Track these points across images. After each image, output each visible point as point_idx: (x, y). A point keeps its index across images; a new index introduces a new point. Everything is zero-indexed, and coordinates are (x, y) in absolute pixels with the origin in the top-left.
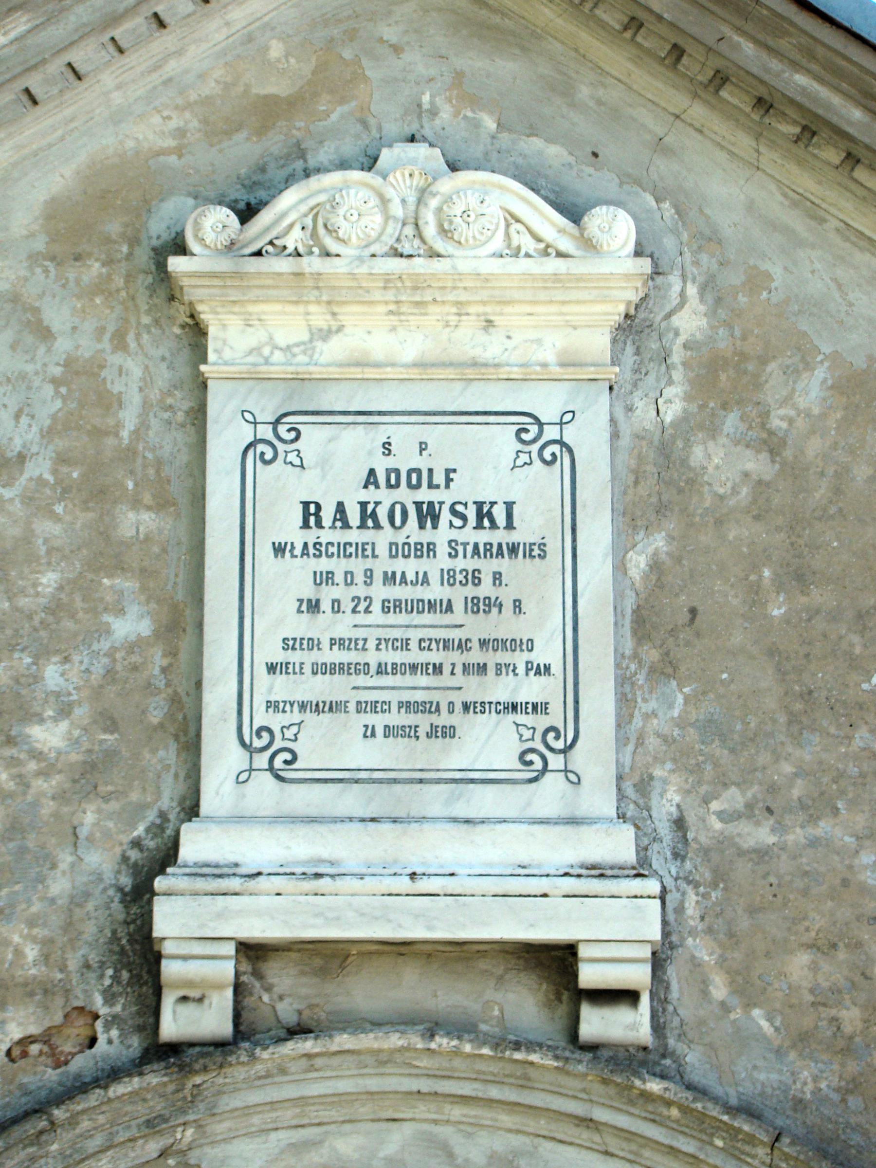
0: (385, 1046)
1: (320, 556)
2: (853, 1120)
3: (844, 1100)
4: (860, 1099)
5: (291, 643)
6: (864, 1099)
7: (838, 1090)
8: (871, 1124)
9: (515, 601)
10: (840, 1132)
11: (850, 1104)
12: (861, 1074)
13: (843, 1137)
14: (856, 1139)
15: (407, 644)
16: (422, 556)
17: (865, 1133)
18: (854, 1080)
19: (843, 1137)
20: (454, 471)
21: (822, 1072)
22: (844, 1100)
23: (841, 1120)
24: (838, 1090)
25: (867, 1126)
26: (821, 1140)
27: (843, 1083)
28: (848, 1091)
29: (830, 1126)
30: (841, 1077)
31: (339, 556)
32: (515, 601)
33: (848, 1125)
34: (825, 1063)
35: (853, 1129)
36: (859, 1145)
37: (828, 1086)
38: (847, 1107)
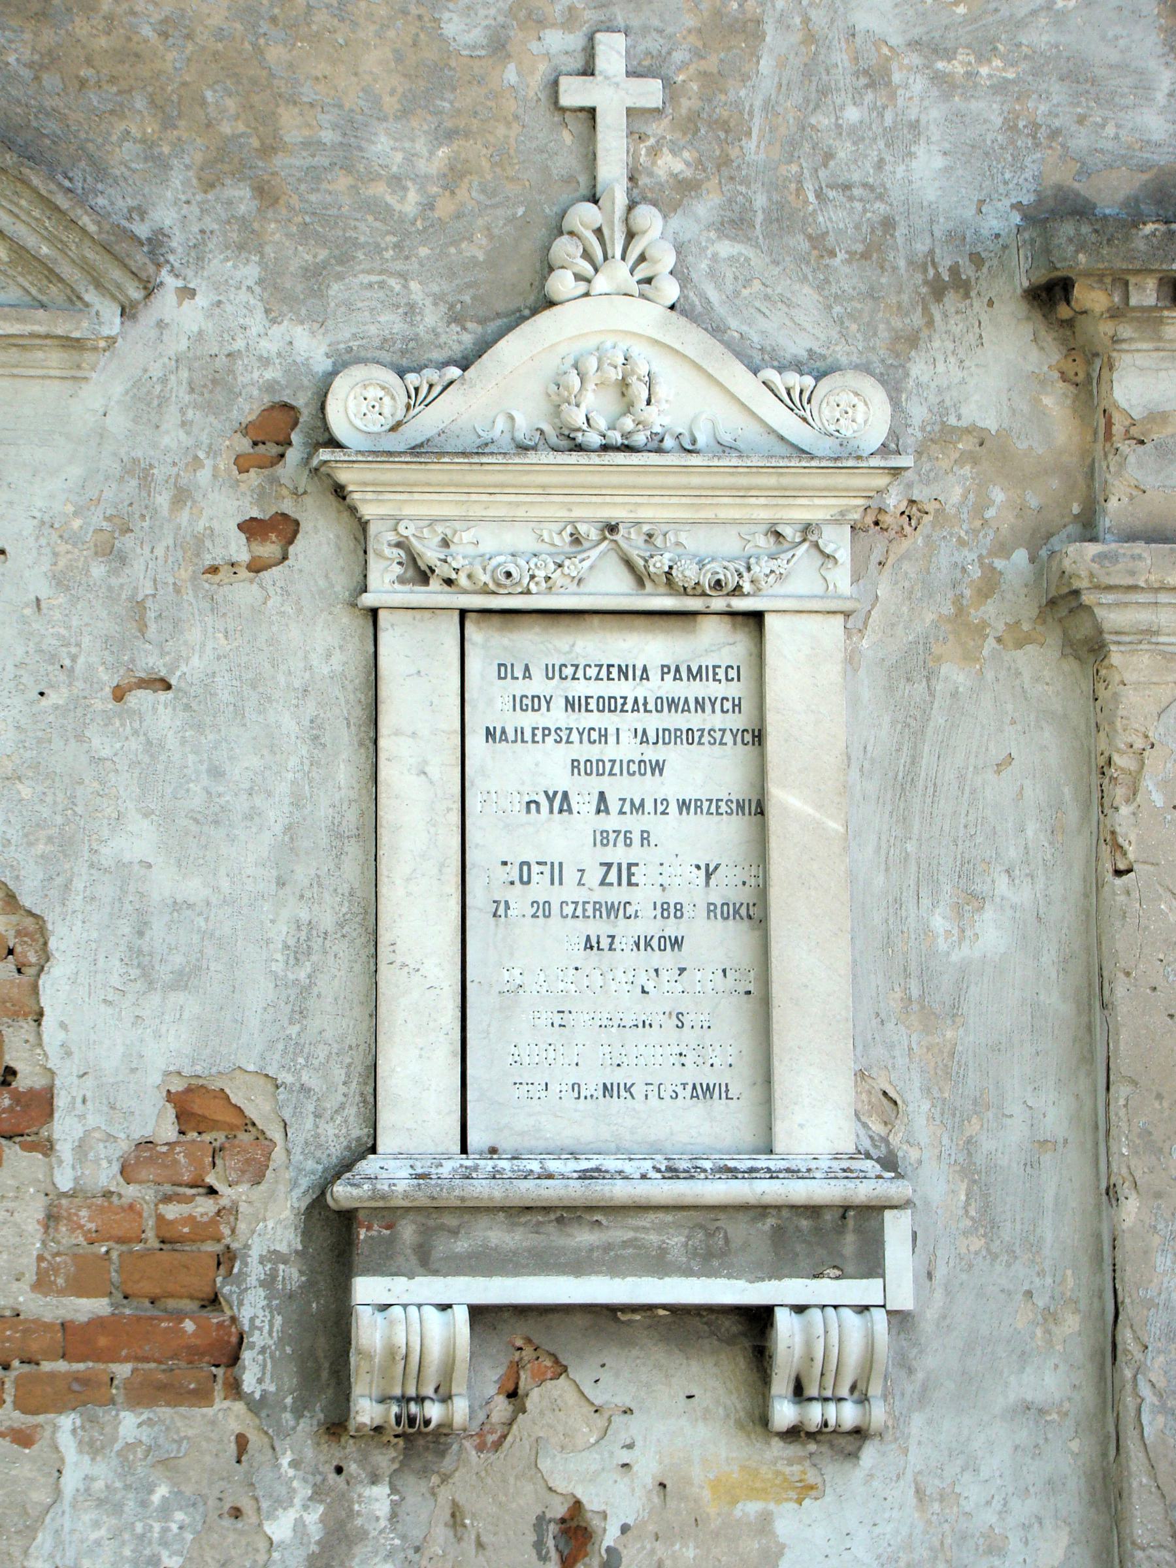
0: (90, 1364)
1: (731, 813)
2: (49, 103)
3: (37, 78)
4: (58, 76)
5: (718, 735)
6: (63, 79)
7: (30, 65)
8: (70, 108)
9: (573, 761)
10: (32, 118)
11: (44, 83)
12: (60, 46)
13: (34, 124)
14: (51, 126)
15: (630, 875)
16: (602, 832)
17: (63, 119)
18: (50, 52)
19: (34, 124)
20: (637, 865)
21: (11, 41)
22: (37, 78)
23: (32, 102)
24: (30, 65)
25: (66, 111)
26: (7, 127)
27: (36, 57)
28: (43, 67)
29: (18, 110)
30: (34, 49)
31: (620, 884)
32: (573, 761)
33: (41, 109)
34: (14, 31)
35: (47, 114)
36: (54, 134)
37: (18, 60)
38: (41, 86)
